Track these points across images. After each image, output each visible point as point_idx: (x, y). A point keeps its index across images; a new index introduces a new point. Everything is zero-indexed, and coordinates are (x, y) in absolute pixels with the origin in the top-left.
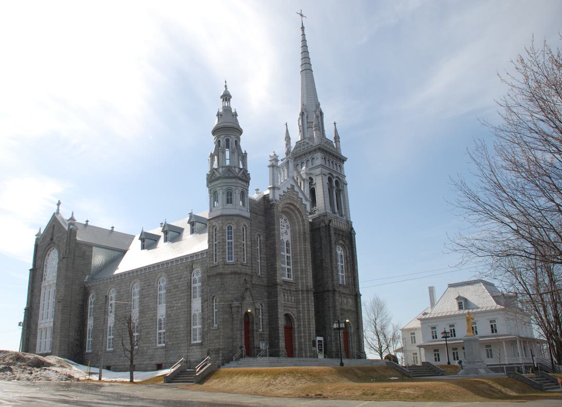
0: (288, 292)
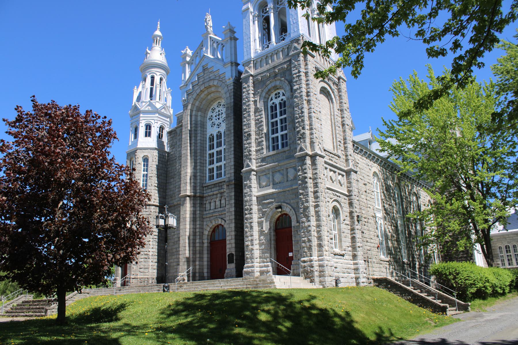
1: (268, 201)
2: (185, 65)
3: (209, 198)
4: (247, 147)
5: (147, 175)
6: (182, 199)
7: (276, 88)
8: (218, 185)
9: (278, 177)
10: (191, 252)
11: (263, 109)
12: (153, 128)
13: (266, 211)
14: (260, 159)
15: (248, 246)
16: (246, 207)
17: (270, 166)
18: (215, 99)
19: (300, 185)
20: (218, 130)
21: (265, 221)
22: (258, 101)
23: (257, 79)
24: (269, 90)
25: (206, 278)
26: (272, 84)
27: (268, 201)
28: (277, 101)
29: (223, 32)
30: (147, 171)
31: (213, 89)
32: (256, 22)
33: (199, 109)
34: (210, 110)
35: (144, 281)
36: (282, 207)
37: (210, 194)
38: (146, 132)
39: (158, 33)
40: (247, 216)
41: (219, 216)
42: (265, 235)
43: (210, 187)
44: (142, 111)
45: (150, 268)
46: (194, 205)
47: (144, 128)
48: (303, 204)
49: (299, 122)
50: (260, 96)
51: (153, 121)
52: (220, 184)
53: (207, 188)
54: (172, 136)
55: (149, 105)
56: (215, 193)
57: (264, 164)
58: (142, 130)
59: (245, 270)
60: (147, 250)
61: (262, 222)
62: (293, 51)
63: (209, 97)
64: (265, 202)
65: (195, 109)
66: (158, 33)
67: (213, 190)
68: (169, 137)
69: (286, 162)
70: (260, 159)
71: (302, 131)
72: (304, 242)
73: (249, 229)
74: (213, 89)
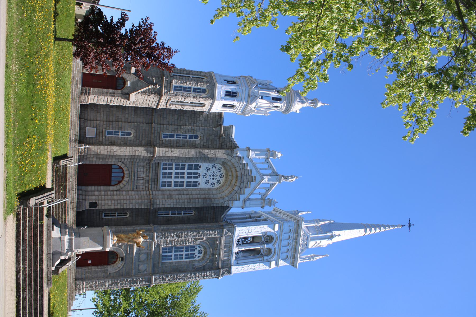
0: (147, 178)
3: (148, 167)
6: (152, 149)
7: (205, 253)
8: (156, 177)
9: (143, 257)
18: (227, 175)
19: (133, 279)
20: (201, 175)
23: (217, 241)
31: (234, 182)
35: (85, 100)
37: (151, 169)
43: (157, 169)
48: (120, 281)
49: (174, 277)
52: (156, 180)
54: (217, 117)
56: (151, 175)
63: (230, 174)
67: (154, 171)
68: (217, 114)
69: (152, 265)
71: (167, 279)
72: (96, 283)
74: (234, 182)
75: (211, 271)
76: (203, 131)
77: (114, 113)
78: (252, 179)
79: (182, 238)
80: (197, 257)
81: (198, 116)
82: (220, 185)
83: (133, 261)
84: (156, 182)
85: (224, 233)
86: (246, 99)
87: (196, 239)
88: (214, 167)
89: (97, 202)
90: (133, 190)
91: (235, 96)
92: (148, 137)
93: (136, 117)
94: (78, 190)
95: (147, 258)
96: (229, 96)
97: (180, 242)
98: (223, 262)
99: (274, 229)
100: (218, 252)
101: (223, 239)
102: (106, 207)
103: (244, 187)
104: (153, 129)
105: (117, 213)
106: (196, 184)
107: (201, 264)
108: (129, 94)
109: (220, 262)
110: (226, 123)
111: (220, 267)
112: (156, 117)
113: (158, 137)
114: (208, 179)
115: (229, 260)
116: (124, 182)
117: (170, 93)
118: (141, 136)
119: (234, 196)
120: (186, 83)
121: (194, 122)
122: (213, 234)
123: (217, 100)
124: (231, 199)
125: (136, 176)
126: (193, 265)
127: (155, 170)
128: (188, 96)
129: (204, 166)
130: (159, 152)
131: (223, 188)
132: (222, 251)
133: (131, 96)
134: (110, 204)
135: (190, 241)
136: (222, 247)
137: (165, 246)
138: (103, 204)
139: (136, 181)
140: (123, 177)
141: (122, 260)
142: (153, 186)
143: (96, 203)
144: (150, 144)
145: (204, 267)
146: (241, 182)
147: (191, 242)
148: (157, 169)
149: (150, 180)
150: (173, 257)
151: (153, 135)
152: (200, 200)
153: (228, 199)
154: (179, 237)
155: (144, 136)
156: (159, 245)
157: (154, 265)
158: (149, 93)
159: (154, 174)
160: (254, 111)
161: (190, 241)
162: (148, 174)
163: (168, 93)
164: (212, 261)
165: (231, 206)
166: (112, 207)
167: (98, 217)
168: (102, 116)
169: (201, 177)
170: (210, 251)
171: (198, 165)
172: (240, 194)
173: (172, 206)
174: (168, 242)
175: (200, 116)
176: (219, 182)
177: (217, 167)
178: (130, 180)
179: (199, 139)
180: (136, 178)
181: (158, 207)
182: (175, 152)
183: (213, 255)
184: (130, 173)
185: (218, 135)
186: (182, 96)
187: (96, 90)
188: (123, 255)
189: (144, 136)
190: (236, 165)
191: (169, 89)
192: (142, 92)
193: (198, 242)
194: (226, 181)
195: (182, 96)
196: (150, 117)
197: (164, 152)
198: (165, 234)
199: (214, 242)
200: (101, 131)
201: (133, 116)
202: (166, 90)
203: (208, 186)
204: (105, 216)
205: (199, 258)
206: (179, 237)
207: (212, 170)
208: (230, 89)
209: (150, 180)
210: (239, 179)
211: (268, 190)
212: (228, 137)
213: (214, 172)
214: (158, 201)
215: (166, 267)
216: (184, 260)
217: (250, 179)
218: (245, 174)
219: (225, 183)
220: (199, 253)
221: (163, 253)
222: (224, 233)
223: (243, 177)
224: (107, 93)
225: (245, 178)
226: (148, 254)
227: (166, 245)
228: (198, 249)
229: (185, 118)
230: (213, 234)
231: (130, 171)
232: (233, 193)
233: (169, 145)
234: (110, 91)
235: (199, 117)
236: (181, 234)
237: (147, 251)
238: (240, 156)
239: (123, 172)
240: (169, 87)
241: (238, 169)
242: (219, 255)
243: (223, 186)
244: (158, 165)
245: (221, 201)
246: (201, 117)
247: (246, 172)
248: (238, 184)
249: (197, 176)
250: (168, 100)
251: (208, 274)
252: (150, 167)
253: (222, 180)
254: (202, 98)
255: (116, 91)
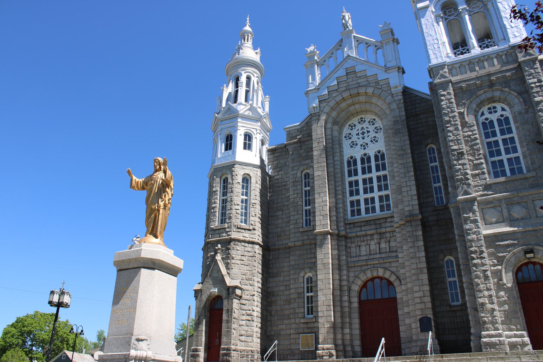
1: (506, 242)
2: (314, 66)
3: (356, 240)
4: (460, 169)
5: (246, 200)
6: (319, 238)
7: (492, 100)
9: (518, 212)
10: (338, 314)
11: (475, 124)
12: (254, 140)
13: (504, 257)
14: (481, 186)
15: (483, 304)
16: (473, 249)
17: (504, 196)
18: (357, 113)
20: (363, 152)
21: (504, 270)
22: (465, 113)
23: (461, 88)
24: (482, 102)
25: (360, 354)
26: (486, 94)
27: (506, 242)
28: (494, 117)
29: (380, 32)
30: (246, 195)
32: (441, 23)
33: (335, 123)
34: (347, 126)
35: (247, 356)
36: (535, 250)
37: (358, 234)
38: (245, 144)
39: (248, 28)
40: (475, 261)
41: (379, 265)
42: (507, 290)
43: (359, 224)
44: (242, 114)
45: (255, 336)
46: (337, 247)
47: (243, 137)
50: (468, 108)
51: (254, 131)
52: (378, 222)
53: (352, 226)
54: (276, 155)
55: (249, 109)
56: (369, 232)
57: (490, 193)
58: (240, 141)
59: (222, 346)
60: (250, 308)
61: (500, 271)
62: (439, 78)
63: (352, 108)
64: (501, 243)
65: (330, 120)
66: (248, 28)
67: (363, 228)
70: (481, 186)
73: (483, 280)
74: (362, 98)
75: (527, 78)
76: (295, 168)
77: (278, 308)
78: (351, 72)
79: (465, 148)
80: (504, 113)
81: (276, 182)
82: (377, 119)
83: (530, 228)
84: (381, 221)
85: (443, 80)
86: (233, 120)
87: (464, 124)
88: (349, 136)
89: (419, 317)
90: (397, 257)
91: (231, 136)
92: (310, 249)
93: (282, 274)
94: (405, 355)
95: (518, 203)
96: (231, 144)
97: (474, 149)
98: (504, 64)
99: (427, 7)
100: (483, 79)
101: (454, 79)
102: (428, 299)
103: (365, 79)
104: (296, 243)
105: (450, 279)
106: (380, 156)
107: (516, 101)
108: (228, 288)
109: (505, 68)
110: (283, 140)
111: (516, 65)
112: (280, 243)
113: (309, 233)
114: (370, 138)
115: (498, 55)
116: (387, 276)
117: (228, 228)
118: (309, 261)
119: (381, 87)
120: (214, 208)
121: (285, 185)
122: (448, 97)
123: (235, 158)
124: (389, 92)
125: (375, 256)
126: (520, 113)
127: (361, 226)
128: (231, 201)
129: (348, 152)
130: (323, 224)
131: (377, 110)
132: (482, 72)
133: (231, 285)
134: (421, 294)
135: (470, 133)
136: (474, 75)
137: (487, 176)
138: (422, 306)
139: (383, 255)
140: (381, 278)
141: (531, 251)
142: (388, 224)
143: (421, 320)
144: (313, 242)
145: (520, 94)
146: (359, 86)
147: (472, 131)
148: (359, 224)
149: (379, 231)
150: (512, 155)
151: (305, 242)
152: (397, 140)
153: (390, 97)
154: (461, 154)
155: (309, 256)
156: (487, 187)
157: (532, 187)
158: (228, 258)
159: (368, 228)
160: (251, 105)
161: (470, 133)
162: (369, 238)
163: (227, 230)
164: (506, 82)
165: (400, 89)
166: (427, 288)
167: (458, 314)
168: (284, 327)
169: (366, 151)
170: (485, 92)
171: (349, 163)
172: (377, 82)
173: (414, 183)
174: (477, 172)
175: (276, 179)
176: (372, 122)
177: (349, 131)
178: (383, 266)
179: (308, 171)
180: (378, 256)
181: (417, 207)
182: (323, 201)
183: (492, 85)
184: (369, 267)
185: (299, 145)
186: (231, 209)
187: (224, 339)
188: (519, 252)
189: (309, 256)
190: (332, 103)
191: (222, 231)
192: (228, 268)
193: (470, 119)
194: (366, 111)
195: (231, 209)
196: (281, 251)
197: (321, 217)
198: (458, 180)
199: (464, 93)
200: (305, 326)
201: (282, 279)
202: (224, 234)
203: (380, 136)
204: (458, 301)
205: (506, 107)
206: (461, 154)
207: (354, 138)
208: (221, 145)
209: (379, 231)
210: (353, 92)
211: (368, 44)
212: (300, 130)
213: (358, 134)
214: (407, 209)
215: (533, 163)
216: (515, 134)
217: (353, 76)
218: (346, 85)
219: (371, 112)
220: (496, 112)
221: (504, 174)
222: (443, 80)
223: (350, 87)
224: (228, 322)
225: (353, 83)
226: (510, 203)
227: (483, 173)
228: (487, 115)
229: (279, 200)
230: (448, 97)
231: (366, 267)
232: (377, 92)
233: (310, 214)
234: (225, 317)
235: (278, 179)
236: (456, 153)
237: (504, 206)
238: (317, 101)
239: (372, 279)
240: (219, 231)
241: (339, 98)
242: (489, 75)
243: (376, 114)
244: (349, 225)
245: (394, 106)
246: (278, 177)
247: (342, 86)
248: (362, 90)
249: (365, 159)
250: (238, 228)
251: (535, 80)
252: (357, 237)
253: (368, 117)
254: (232, 180)
255: (224, 308)
